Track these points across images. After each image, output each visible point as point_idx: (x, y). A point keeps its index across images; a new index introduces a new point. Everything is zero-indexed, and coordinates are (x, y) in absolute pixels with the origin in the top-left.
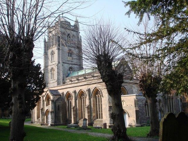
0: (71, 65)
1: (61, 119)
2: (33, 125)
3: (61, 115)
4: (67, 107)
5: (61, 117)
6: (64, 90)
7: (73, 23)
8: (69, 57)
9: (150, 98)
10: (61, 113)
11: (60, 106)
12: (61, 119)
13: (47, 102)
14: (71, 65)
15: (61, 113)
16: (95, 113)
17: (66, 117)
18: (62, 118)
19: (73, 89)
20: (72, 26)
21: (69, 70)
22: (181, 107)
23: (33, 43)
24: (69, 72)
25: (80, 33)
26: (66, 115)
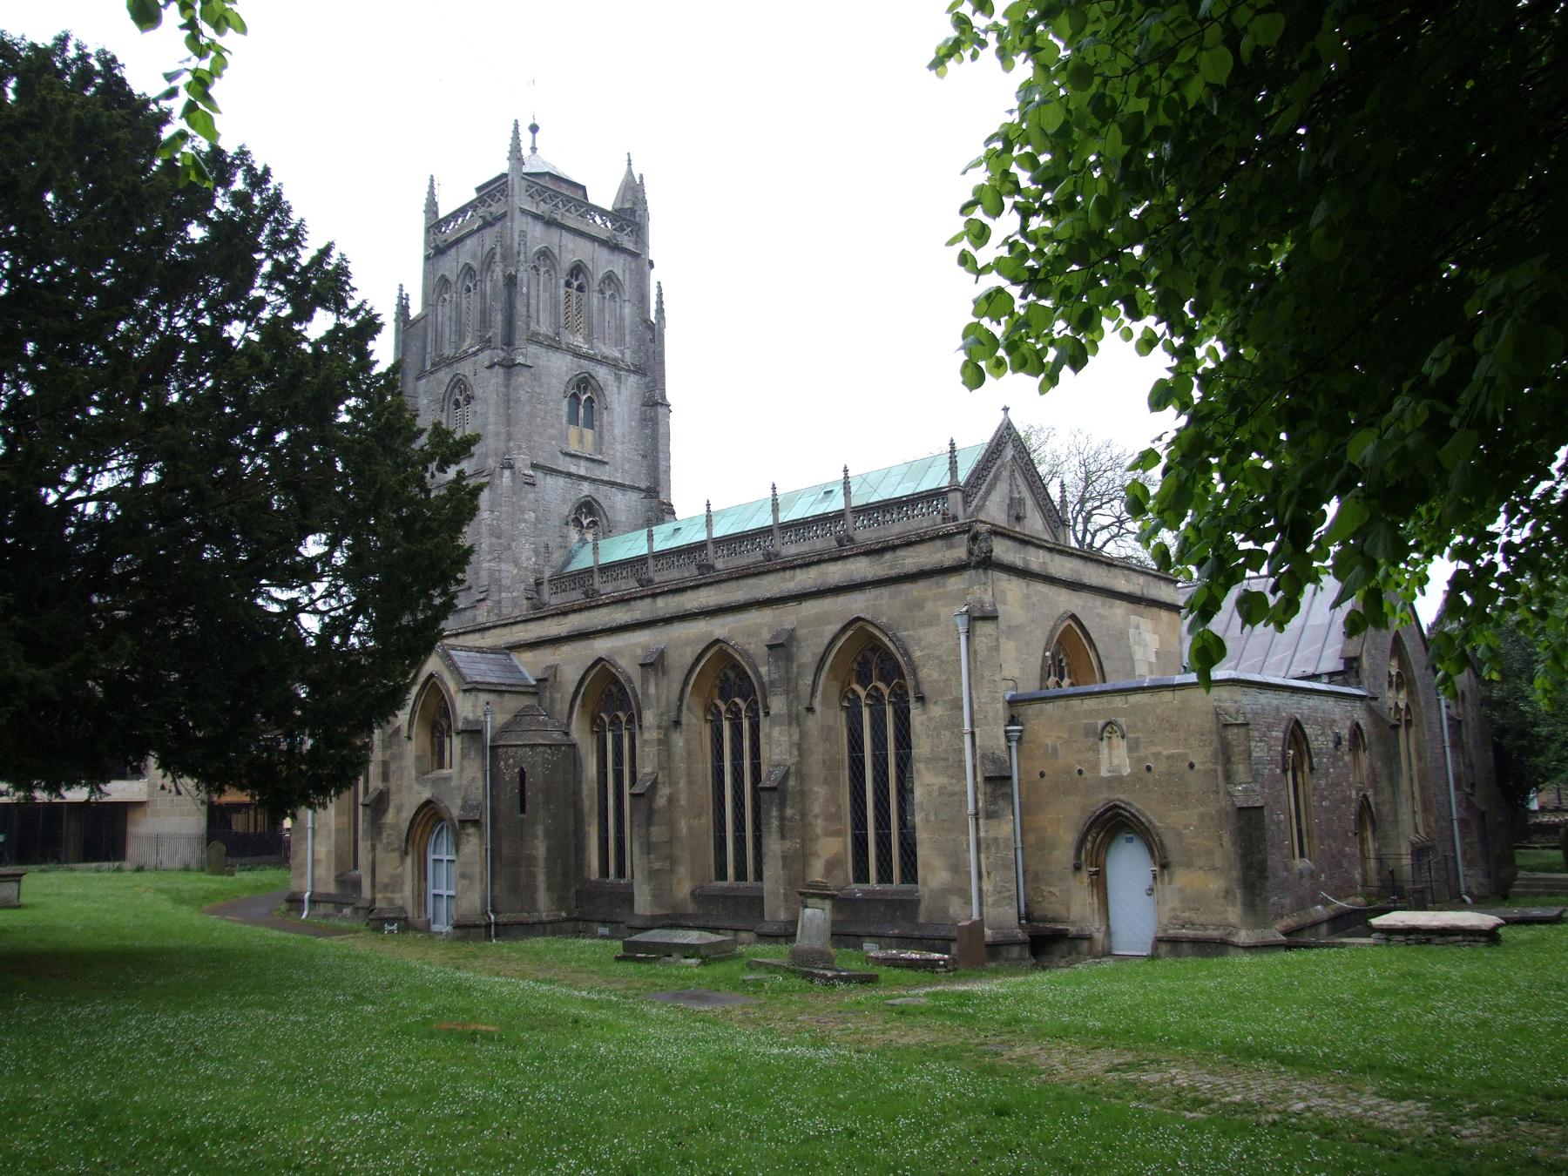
0: (586, 489)
1: (541, 879)
2: (106, 799)
3: (541, 849)
4: (585, 792)
5: (541, 863)
6: (566, 649)
7: (604, 195)
8: (573, 430)
9: (227, 787)
10: (540, 830)
11: (529, 780)
12: (541, 879)
13: (427, 742)
14: (586, 489)
15: (540, 830)
16: (837, 833)
17: (581, 864)
18: (550, 873)
19: (763, 623)
20: (602, 212)
21: (578, 522)
22: (1457, 788)
23: (314, 311)
24: (574, 535)
25: (651, 264)
26: (580, 849)
